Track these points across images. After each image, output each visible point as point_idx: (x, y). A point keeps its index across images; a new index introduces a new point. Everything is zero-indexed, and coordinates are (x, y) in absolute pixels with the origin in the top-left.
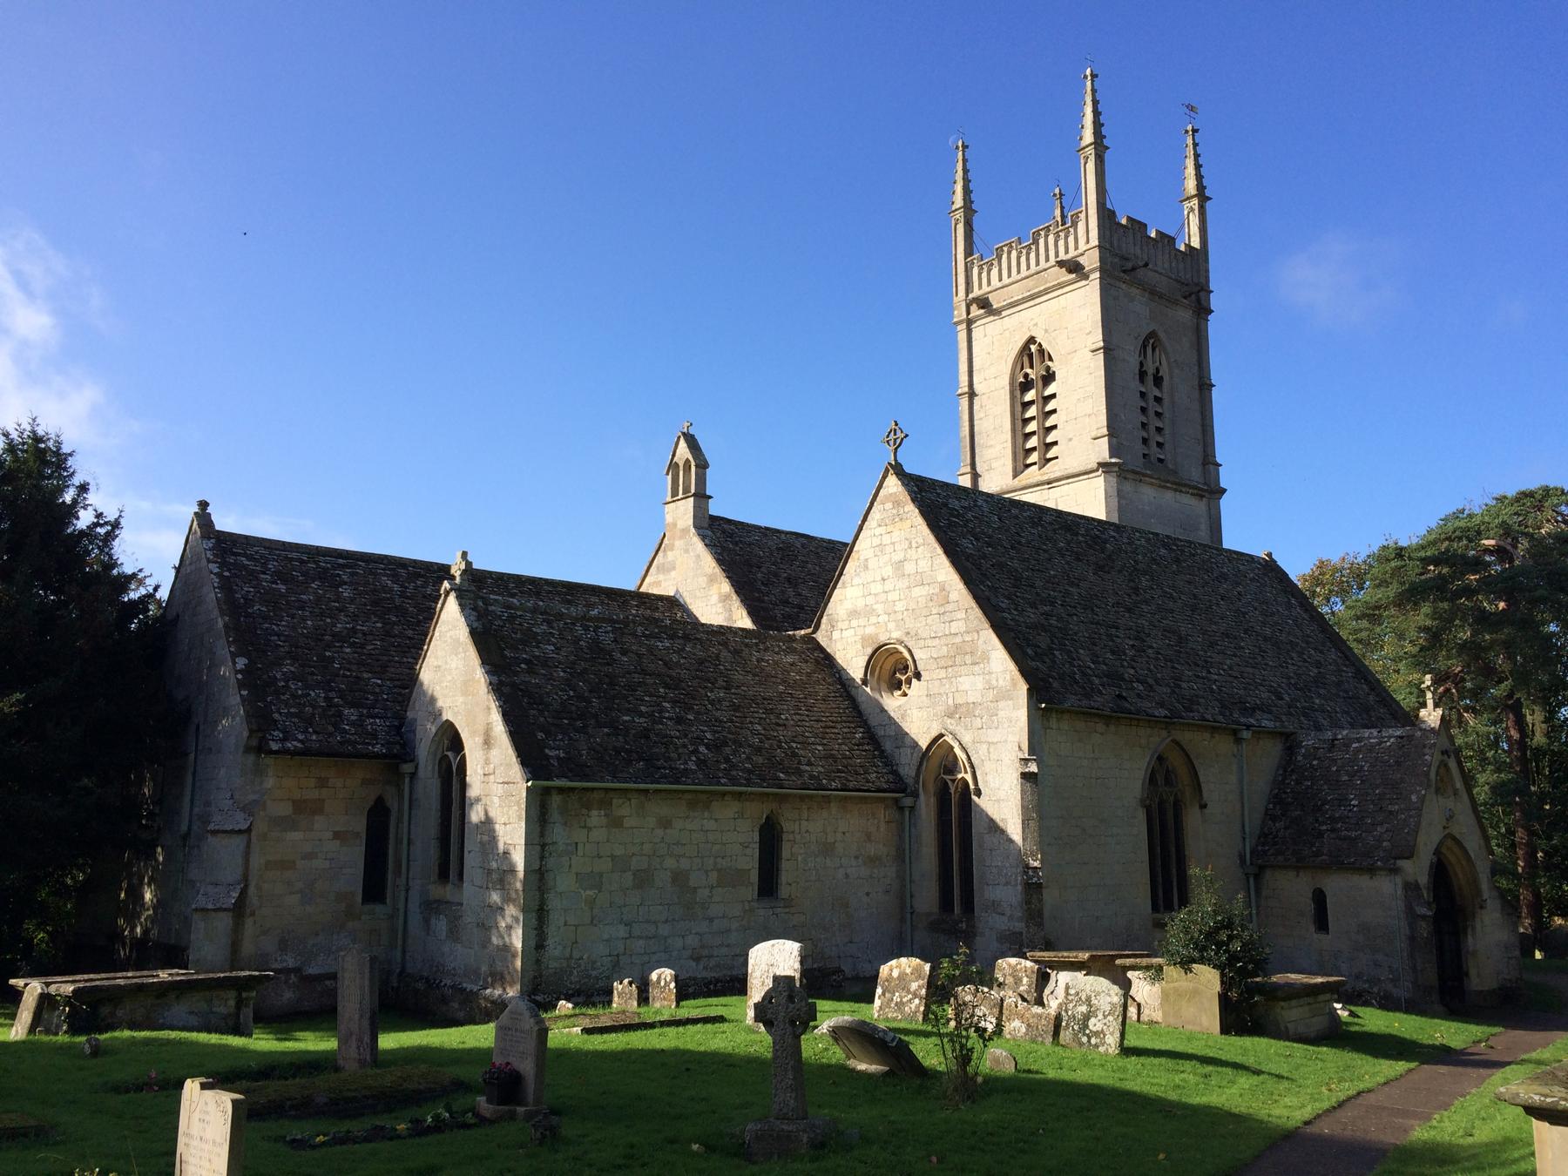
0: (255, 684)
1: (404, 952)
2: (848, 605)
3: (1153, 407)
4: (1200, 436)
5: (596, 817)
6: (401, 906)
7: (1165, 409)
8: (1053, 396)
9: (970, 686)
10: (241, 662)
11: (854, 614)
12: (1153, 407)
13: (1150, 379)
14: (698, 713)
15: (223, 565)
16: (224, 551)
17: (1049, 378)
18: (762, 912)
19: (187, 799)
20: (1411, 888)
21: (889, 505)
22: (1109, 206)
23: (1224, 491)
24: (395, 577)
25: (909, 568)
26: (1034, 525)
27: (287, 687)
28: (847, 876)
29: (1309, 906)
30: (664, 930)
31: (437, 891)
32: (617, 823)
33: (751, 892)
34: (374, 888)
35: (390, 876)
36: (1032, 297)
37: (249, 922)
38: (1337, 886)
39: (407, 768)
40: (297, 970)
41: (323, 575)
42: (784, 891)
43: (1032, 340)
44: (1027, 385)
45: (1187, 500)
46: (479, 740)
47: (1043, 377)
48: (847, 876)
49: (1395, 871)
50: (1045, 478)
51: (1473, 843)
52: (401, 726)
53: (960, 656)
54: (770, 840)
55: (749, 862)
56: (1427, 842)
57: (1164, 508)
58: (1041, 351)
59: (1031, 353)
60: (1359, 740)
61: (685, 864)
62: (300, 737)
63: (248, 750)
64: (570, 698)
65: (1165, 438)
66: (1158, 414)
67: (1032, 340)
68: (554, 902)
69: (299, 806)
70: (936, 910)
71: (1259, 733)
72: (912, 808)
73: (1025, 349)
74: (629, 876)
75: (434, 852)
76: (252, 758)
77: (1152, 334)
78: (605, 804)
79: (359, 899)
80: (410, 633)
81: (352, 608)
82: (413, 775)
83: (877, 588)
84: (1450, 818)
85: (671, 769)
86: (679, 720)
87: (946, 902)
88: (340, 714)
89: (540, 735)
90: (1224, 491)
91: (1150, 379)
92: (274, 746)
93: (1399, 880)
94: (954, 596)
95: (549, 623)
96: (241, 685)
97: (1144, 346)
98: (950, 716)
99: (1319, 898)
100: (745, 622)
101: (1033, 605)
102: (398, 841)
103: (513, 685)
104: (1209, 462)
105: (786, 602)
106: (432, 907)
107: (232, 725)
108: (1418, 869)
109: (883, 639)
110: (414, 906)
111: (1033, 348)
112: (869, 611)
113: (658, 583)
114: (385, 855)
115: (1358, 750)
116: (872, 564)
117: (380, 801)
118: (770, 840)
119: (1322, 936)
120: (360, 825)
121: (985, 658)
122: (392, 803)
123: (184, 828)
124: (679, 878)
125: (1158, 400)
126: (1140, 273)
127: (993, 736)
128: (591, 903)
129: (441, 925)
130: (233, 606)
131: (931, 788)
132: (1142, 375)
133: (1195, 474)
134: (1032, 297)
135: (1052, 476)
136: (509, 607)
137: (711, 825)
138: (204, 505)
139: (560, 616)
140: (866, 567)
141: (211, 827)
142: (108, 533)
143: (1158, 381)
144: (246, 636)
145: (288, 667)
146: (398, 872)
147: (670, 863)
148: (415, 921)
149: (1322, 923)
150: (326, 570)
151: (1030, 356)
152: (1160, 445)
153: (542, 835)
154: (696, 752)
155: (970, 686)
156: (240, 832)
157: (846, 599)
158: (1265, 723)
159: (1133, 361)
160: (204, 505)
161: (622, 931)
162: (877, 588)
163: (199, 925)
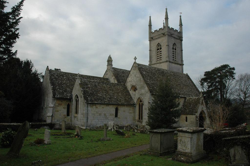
0: (54, 89)
1: (72, 122)
2: (129, 80)
3: (175, 53)
4: (181, 57)
5: (94, 107)
6: (71, 116)
7: (176, 53)
8: (161, 51)
9: (143, 91)
10: (52, 86)
11: (130, 81)
12: (175, 53)
13: (174, 49)
14: (108, 94)
15: (50, 74)
16: (50, 72)
17: (161, 49)
18: (116, 119)
19: (46, 103)
20: (197, 117)
21: (134, 67)
22: (169, 26)
23: (184, 64)
24: (71, 76)
25: (136, 76)
26: (154, 70)
27: (57, 89)
28: (127, 115)
29: (185, 119)
30: (103, 121)
31: (75, 115)
32: (97, 108)
33: (114, 116)
34: (68, 115)
35: (70, 113)
36: (159, 38)
37: (53, 118)
38: (189, 116)
39: (72, 100)
40: (59, 124)
41: (62, 75)
42: (118, 116)
43: (159, 43)
44: (158, 49)
45: (179, 66)
46: (80, 97)
47: (160, 48)
48: (127, 115)
49: (195, 114)
50: (160, 62)
51: (205, 111)
52: (71, 95)
53: (142, 87)
54: (117, 110)
55: (114, 113)
56: (199, 111)
57: (175, 68)
58: (160, 45)
59: (159, 45)
60: (193, 98)
61: (106, 113)
62: (59, 96)
63: (53, 97)
64: (92, 92)
65: (176, 57)
66: (175, 54)
67: (159, 43)
68: (89, 117)
69: (59, 104)
70: (138, 119)
71: (181, 97)
72: (136, 106)
73: (158, 44)
74: (98, 114)
75: (75, 110)
76: (53, 98)
77: (175, 43)
78: (95, 105)
79: (66, 116)
80: (73, 83)
81: (66, 80)
82: (72, 101)
83: (132, 78)
84: (202, 108)
85: (104, 101)
86: (106, 95)
87: (139, 119)
88: (64, 93)
89: (87, 97)
90: (184, 64)
91: (174, 49)
92: (56, 97)
93: (195, 116)
94: (142, 80)
95: (89, 82)
96: (52, 89)
97: (173, 45)
98: (141, 95)
99: (186, 118)
100: (116, 82)
101: (152, 81)
102: (71, 109)
103: (84, 90)
104: (182, 61)
105: (122, 79)
106: (75, 117)
107: (51, 95)
108: (198, 114)
109: (133, 85)
110: (73, 117)
111: (159, 44)
112: (131, 81)
113: (106, 76)
114: (69, 111)
115: (193, 100)
116: (132, 75)
117: (69, 104)
118: (117, 110)
119: (186, 122)
120: (66, 107)
121: (145, 88)
122: (70, 104)
123: (46, 106)
124: (105, 114)
125: (175, 52)
126: (173, 35)
127: (145, 98)
128: (94, 117)
129: (76, 119)
130: (51, 79)
131: (138, 104)
132: (173, 49)
133: (180, 63)
134: (159, 38)
135: (161, 62)
136: (84, 80)
137: (109, 108)
138: (48, 66)
139: (91, 81)
140: (131, 75)
141: (49, 106)
142: (13, 23)
143: (175, 49)
144: (53, 84)
145: (58, 87)
146: (71, 113)
147: (104, 113)
148: (73, 119)
149: (187, 121)
150: (62, 75)
151: (159, 46)
152: (175, 58)
153: (87, 109)
154: (107, 99)
155: (143, 91)
156: (52, 107)
157: (129, 79)
158: (182, 96)
159: (172, 47)
160: (48, 66)
161: (98, 121)
162: (132, 78)
163: (47, 118)
